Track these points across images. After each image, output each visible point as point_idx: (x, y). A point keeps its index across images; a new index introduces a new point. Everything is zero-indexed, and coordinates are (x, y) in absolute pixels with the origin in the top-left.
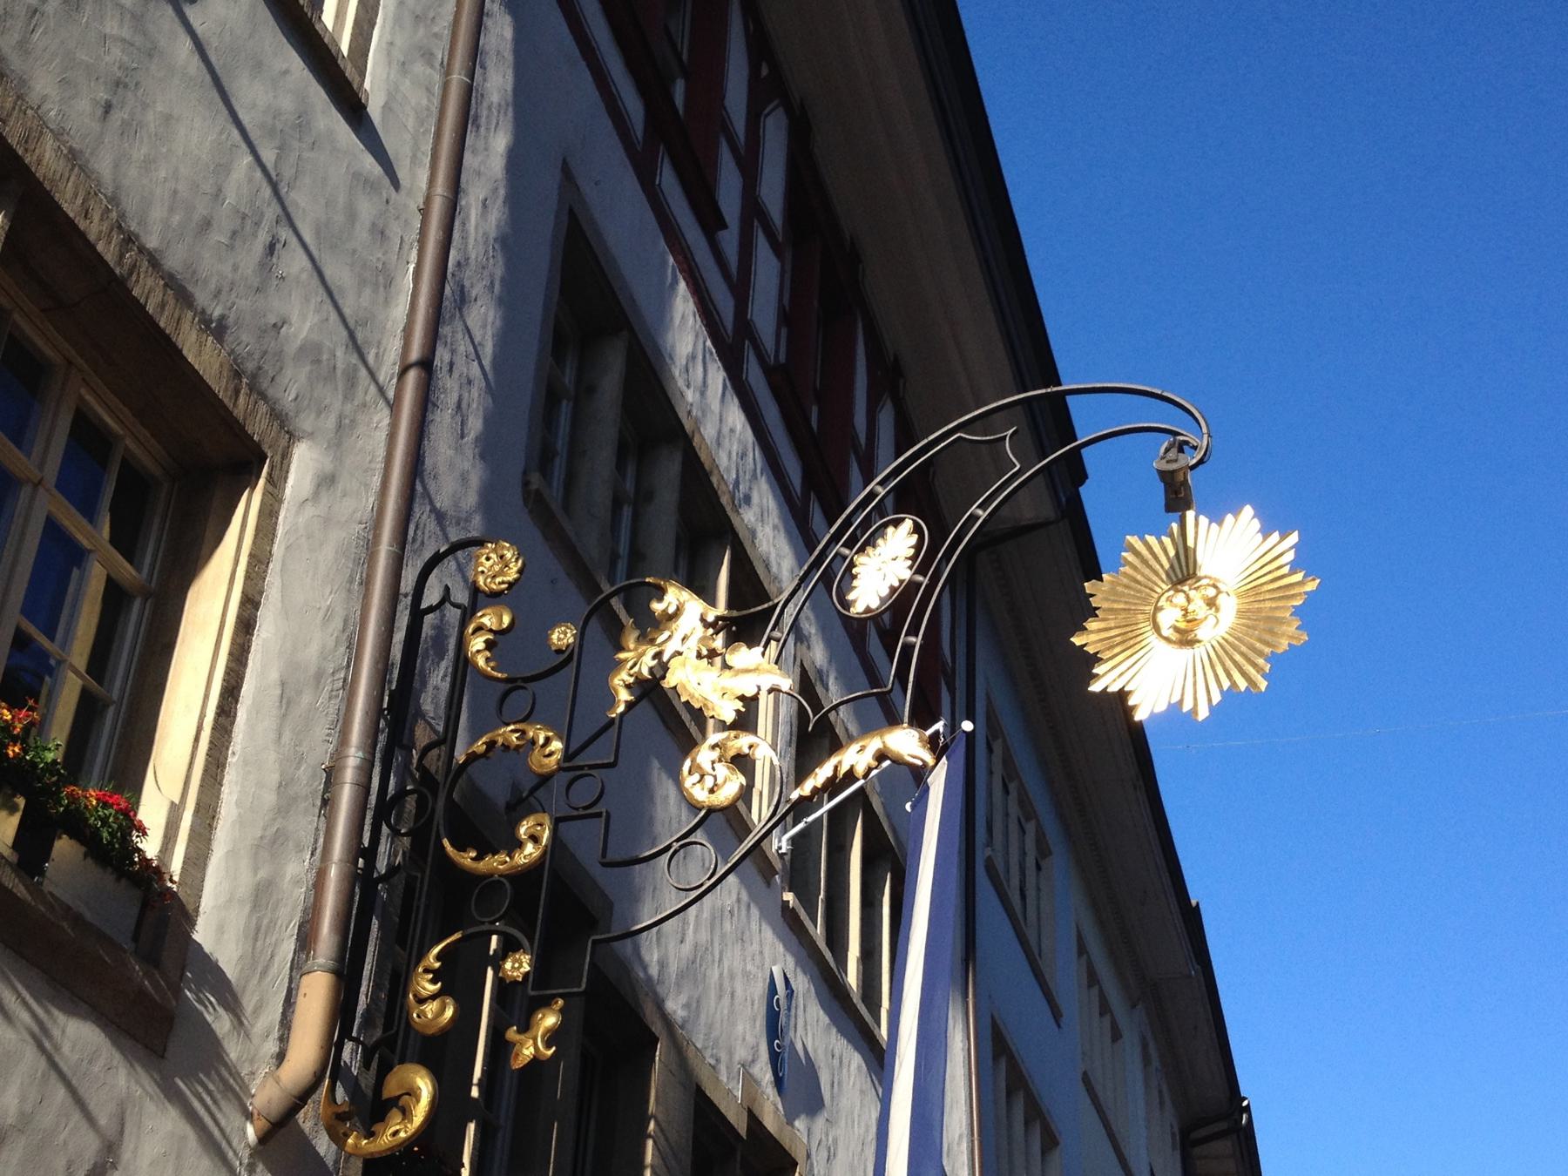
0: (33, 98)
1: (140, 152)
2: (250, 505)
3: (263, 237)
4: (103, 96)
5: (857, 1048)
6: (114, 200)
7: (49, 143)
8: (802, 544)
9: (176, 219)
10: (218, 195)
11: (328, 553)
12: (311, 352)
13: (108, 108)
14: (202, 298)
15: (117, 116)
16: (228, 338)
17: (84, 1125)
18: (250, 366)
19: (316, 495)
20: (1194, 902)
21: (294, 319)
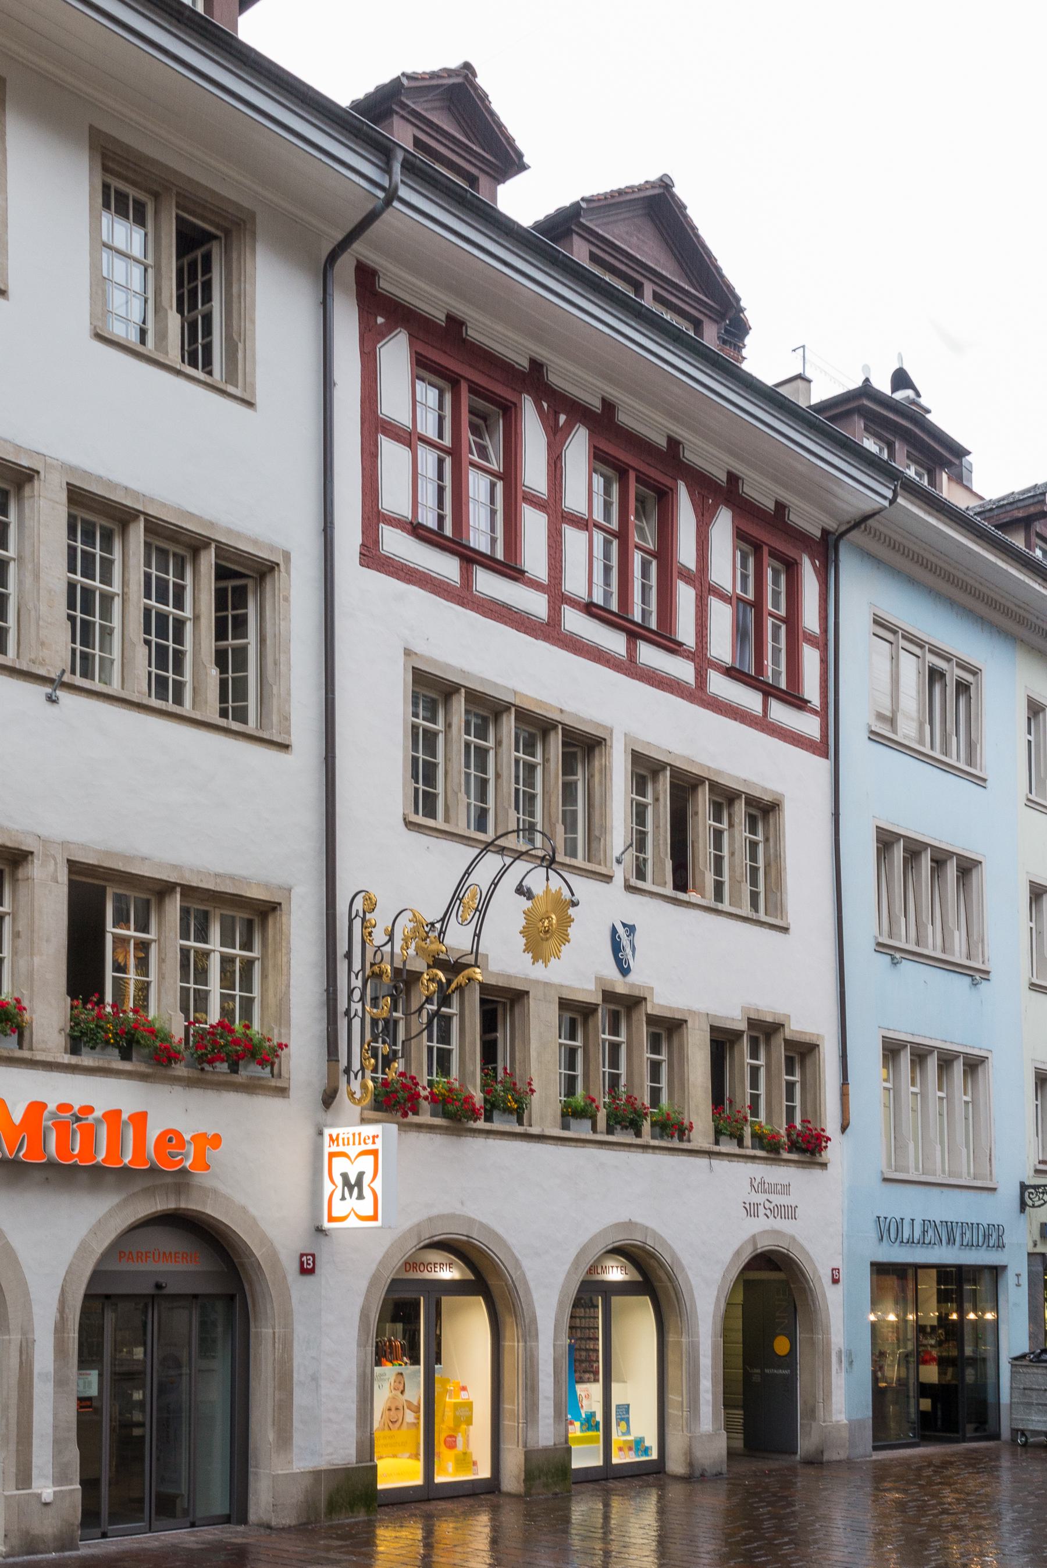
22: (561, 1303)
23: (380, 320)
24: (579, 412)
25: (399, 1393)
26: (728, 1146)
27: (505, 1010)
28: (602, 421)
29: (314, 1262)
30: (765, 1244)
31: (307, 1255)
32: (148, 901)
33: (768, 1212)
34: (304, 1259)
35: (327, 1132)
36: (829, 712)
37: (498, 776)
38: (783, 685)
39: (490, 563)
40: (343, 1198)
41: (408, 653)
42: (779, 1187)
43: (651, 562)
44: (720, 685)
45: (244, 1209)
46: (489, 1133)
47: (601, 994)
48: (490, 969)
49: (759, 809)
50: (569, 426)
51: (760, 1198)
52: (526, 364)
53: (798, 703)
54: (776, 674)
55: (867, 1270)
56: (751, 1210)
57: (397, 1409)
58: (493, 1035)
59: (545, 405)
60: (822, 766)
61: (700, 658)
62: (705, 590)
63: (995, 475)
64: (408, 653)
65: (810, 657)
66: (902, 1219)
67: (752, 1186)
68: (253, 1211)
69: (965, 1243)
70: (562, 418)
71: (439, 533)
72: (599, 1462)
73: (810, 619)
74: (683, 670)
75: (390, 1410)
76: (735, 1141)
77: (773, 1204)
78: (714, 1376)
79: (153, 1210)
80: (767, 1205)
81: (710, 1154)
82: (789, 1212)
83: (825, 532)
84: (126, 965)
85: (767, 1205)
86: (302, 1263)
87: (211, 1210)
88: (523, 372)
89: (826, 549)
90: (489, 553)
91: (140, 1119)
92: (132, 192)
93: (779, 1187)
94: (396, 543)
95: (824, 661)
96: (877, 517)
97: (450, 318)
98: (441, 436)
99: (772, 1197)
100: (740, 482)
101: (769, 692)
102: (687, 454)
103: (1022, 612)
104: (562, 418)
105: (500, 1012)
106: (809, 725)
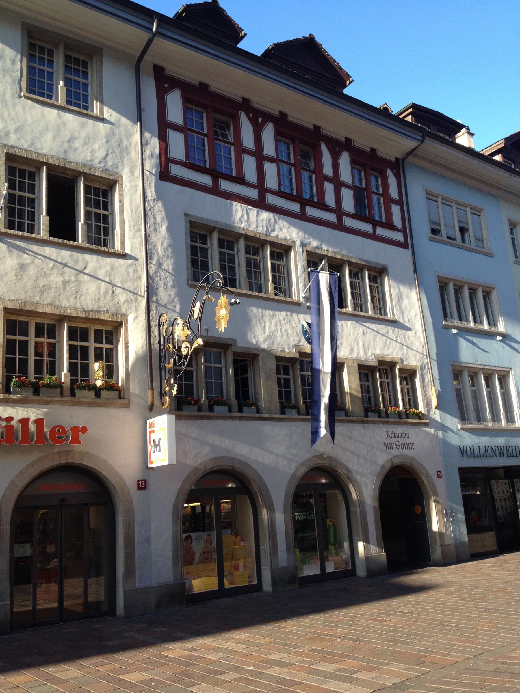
0: (64, 306)
1: (84, 298)
2: (123, 330)
3: (110, 292)
4: (74, 296)
5: (389, 326)
6: (82, 308)
7: (68, 309)
8: (342, 279)
9: (93, 302)
10: (100, 293)
11: (139, 328)
12: (127, 301)
13: (76, 297)
14: (102, 309)
15: (78, 297)
16: (109, 311)
17: (419, 147)
18: (115, 312)
19: (134, 321)
20: (312, 127)
21: (121, 299)
22: (286, 496)
23: (166, 85)
24: (268, 117)
25: (208, 544)
26: (372, 417)
27: (250, 363)
28: (347, 145)
29: (145, 484)
30: (396, 461)
31: (141, 480)
32: (220, 353)
33: (398, 447)
34: (140, 482)
35: (148, 421)
36: (406, 229)
37: (239, 264)
38: (234, 174)
39: (230, 178)
40: (154, 452)
41: (186, 215)
42: (403, 435)
43: (230, 148)
44: (348, 222)
45: (105, 461)
46: (241, 418)
47: (298, 354)
48: (238, 345)
49: (377, 272)
50: (263, 124)
51: (393, 440)
52: (344, 140)
53: (392, 227)
54: (381, 217)
55: (457, 471)
56: (389, 446)
57: (208, 552)
58: (246, 375)
59: (251, 115)
60: (407, 253)
61: (339, 211)
62: (338, 184)
63: (482, 136)
64: (186, 215)
65: (396, 210)
66: (473, 446)
67: (387, 435)
68: (110, 461)
69: (509, 455)
70: (260, 120)
71: (291, 194)
72: (318, 572)
73: (394, 193)
74: (332, 218)
75: (204, 553)
76: (377, 414)
77: (400, 443)
78: (376, 526)
79: (53, 464)
80: (397, 443)
81: (363, 422)
82: (411, 446)
83: (397, 159)
84: (43, 353)
85: (397, 443)
86: (138, 485)
87: (86, 462)
88: (239, 103)
89: (398, 166)
90: (229, 174)
91: (39, 422)
92: (46, 46)
93: (403, 435)
94: (176, 170)
95: (402, 210)
96: (417, 149)
97: (315, 126)
98: (289, 159)
99: (399, 440)
100: (352, 141)
101: (375, 224)
102: (324, 131)
103: (499, 185)
104: (260, 120)
105: (248, 365)
106: (399, 237)
